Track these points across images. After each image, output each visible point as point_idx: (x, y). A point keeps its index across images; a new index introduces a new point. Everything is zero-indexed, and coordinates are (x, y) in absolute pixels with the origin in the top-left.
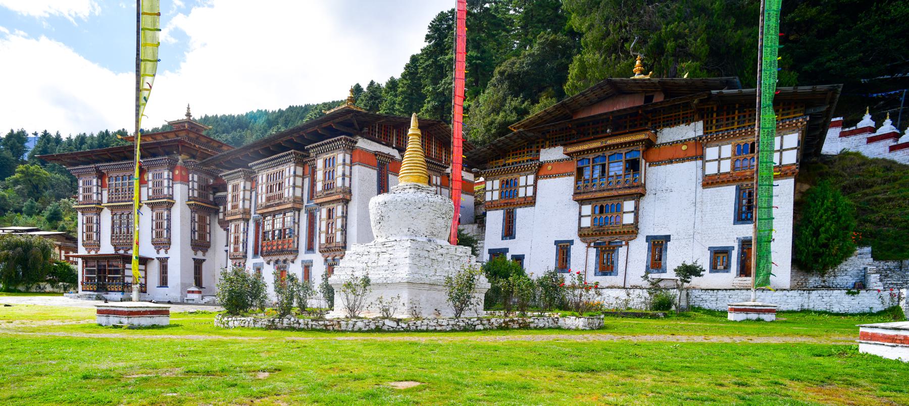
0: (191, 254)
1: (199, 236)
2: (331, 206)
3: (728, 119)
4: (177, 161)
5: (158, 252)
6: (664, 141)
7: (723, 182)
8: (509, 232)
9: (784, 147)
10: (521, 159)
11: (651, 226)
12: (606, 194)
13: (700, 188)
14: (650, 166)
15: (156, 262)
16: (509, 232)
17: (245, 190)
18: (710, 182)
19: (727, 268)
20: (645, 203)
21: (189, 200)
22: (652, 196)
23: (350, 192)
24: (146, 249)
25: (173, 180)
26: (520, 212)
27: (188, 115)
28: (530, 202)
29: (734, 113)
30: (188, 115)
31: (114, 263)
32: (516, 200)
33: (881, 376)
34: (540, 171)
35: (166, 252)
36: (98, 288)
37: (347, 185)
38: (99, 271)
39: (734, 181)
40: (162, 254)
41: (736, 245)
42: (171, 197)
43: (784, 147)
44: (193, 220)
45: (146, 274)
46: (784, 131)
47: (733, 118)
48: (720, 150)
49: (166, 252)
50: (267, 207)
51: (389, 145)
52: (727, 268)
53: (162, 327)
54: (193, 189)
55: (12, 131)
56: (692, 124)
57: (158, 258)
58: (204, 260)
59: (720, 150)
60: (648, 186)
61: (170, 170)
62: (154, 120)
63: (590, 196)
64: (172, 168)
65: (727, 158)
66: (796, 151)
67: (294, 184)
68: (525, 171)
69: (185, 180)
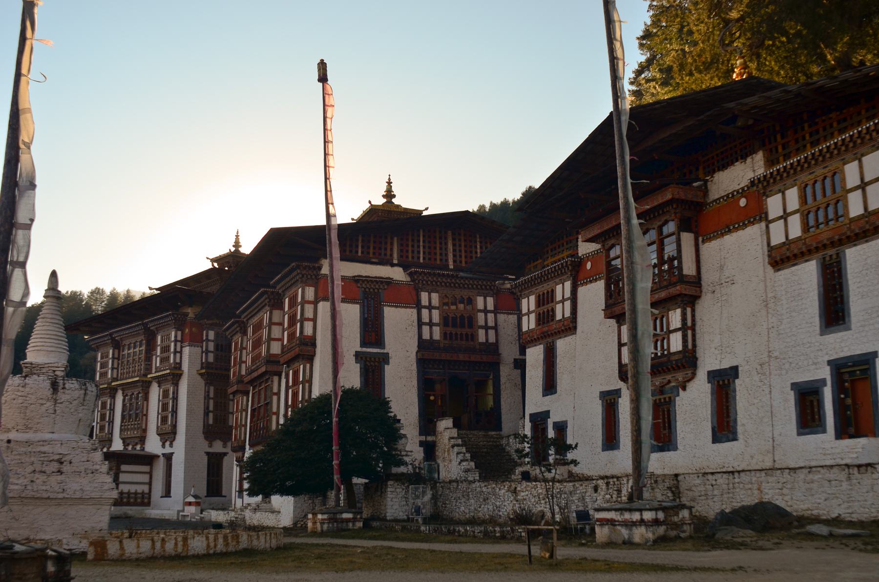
0: (203, 446)
1: (215, 419)
3: (797, 141)
4: (187, 315)
5: (210, 446)
6: (717, 197)
7: (795, 256)
9: (867, 180)
10: (561, 256)
11: (710, 360)
13: (770, 269)
14: (704, 242)
15: (162, 459)
16: (550, 386)
18: (781, 258)
20: (706, 308)
21: (202, 368)
22: (709, 295)
23: (314, 345)
24: (153, 445)
25: (182, 342)
26: (561, 344)
27: (389, 195)
29: (803, 129)
30: (389, 195)
32: (554, 326)
35: (171, 446)
37: (178, 360)
39: (810, 252)
40: (168, 450)
42: (178, 366)
43: (867, 180)
44: (207, 397)
45: (151, 478)
46: (862, 150)
47: (804, 138)
48: (784, 199)
49: (171, 446)
51: (386, 262)
53: (677, 569)
54: (431, 324)
56: (749, 160)
57: (164, 454)
59: (784, 199)
60: (708, 277)
61: (177, 329)
62: (349, 211)
64: (179, 327)
65: (774, 220)
67: (207, 349)
68: (557, 275)
69: (195, 340)
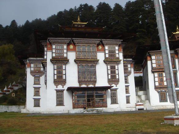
38: (88, 96)
58: (117, 89)
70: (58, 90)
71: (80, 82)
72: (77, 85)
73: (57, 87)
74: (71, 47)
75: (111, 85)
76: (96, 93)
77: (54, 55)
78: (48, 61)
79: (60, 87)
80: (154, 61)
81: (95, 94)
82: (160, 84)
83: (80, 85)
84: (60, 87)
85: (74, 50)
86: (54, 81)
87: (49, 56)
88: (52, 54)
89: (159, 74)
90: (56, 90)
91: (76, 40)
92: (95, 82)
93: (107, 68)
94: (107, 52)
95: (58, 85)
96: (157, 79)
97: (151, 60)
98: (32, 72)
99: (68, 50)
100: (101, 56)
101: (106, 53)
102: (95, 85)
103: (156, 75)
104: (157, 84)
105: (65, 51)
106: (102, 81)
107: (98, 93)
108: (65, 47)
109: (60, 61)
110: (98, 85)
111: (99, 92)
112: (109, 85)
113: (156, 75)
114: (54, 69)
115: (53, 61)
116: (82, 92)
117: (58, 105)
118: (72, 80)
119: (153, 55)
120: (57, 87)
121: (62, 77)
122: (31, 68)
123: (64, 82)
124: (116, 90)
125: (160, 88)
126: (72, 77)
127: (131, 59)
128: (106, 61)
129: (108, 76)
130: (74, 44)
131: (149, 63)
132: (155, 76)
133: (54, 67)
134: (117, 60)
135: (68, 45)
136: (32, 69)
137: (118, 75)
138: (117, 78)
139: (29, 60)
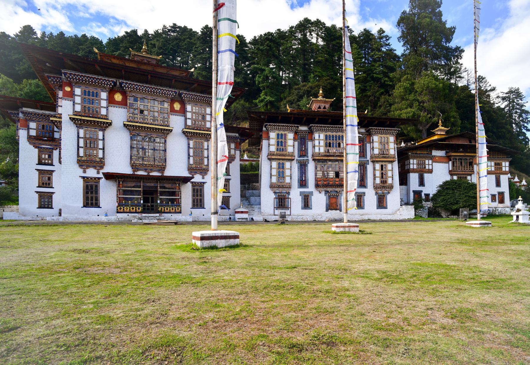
2: (383, 163)
8: (422, 183)
12: (464, 173)
16: (422, 183)
17: (319, 146)
19: (495, 201)
26: (426, 175)
28: (430, 171)
30: (231, 84)
31: (167, 186)
33: (197, 202)
34: (434, 159)
36: (144, 209)
38: (145, 192)
40: (198, 178)
41: (497, 194)
50: (277, 155)
52: (495, 201)
55: (255, 37)
58: (204, 183)
63: (456, 173)
66: (35, 131)
70: (88, 178)
71: (134, 167)
72: (128, 171)
73: (85, 172)
74: (118, 97)
75: (149, 173)
76: (161, 187)
77: (78, 108)
78: (65, 119)
79: (92, 173)
80: (376, 145)
81: (159, 190)
82: (278, 181)
83: (134, 171)
84: (92, 173)
85: (123, 103)
86: (188, 167)
87: (66, 108)
88: (74, 105)
89: (279, 164)
90: (83, 178)
91: (127, 84)
92: (162, 169)
93: (189, 144)
94: (189, 115)
95: (87, 168)
96: (274, 172)
97: (268, 138)
98: (30, 138)
99: (111, 101)
100: (177, 123)
101: (188, 117)
102: (163, 173)
103: (275, 164)
104: (274, 180)
105: (104, 103)
106: (177, 165)
107: (164, 188)
108: (104, 95)
109: (91, 122)
110: (169, 172)
111: (167, 186)
112: (191, 176)
113: (275, 164)
114: (78, 136)
115: (78, 121)
116: (133, 184)
117: (86, 205)
118: (119, 161)
119: (376, 134)
120: (85, 172)
121: (202, 160)
122: (271, 140)
123: (100, 164)
124: (202, 184)
125: (279, 187)
126: (118, 152)
127: (237, 135)
128: (188, 134)
129: (189, 158)
130: (124, 94)
131: (264, 143)
132: (273, 167)
133: (78, 133)
134: (207, 132)
135: (111, 93)
136: (33, 133)
137: (208, 160)
138: (206, 163)
139: (22, 112)
